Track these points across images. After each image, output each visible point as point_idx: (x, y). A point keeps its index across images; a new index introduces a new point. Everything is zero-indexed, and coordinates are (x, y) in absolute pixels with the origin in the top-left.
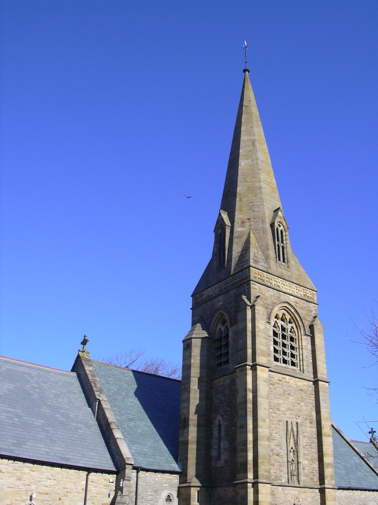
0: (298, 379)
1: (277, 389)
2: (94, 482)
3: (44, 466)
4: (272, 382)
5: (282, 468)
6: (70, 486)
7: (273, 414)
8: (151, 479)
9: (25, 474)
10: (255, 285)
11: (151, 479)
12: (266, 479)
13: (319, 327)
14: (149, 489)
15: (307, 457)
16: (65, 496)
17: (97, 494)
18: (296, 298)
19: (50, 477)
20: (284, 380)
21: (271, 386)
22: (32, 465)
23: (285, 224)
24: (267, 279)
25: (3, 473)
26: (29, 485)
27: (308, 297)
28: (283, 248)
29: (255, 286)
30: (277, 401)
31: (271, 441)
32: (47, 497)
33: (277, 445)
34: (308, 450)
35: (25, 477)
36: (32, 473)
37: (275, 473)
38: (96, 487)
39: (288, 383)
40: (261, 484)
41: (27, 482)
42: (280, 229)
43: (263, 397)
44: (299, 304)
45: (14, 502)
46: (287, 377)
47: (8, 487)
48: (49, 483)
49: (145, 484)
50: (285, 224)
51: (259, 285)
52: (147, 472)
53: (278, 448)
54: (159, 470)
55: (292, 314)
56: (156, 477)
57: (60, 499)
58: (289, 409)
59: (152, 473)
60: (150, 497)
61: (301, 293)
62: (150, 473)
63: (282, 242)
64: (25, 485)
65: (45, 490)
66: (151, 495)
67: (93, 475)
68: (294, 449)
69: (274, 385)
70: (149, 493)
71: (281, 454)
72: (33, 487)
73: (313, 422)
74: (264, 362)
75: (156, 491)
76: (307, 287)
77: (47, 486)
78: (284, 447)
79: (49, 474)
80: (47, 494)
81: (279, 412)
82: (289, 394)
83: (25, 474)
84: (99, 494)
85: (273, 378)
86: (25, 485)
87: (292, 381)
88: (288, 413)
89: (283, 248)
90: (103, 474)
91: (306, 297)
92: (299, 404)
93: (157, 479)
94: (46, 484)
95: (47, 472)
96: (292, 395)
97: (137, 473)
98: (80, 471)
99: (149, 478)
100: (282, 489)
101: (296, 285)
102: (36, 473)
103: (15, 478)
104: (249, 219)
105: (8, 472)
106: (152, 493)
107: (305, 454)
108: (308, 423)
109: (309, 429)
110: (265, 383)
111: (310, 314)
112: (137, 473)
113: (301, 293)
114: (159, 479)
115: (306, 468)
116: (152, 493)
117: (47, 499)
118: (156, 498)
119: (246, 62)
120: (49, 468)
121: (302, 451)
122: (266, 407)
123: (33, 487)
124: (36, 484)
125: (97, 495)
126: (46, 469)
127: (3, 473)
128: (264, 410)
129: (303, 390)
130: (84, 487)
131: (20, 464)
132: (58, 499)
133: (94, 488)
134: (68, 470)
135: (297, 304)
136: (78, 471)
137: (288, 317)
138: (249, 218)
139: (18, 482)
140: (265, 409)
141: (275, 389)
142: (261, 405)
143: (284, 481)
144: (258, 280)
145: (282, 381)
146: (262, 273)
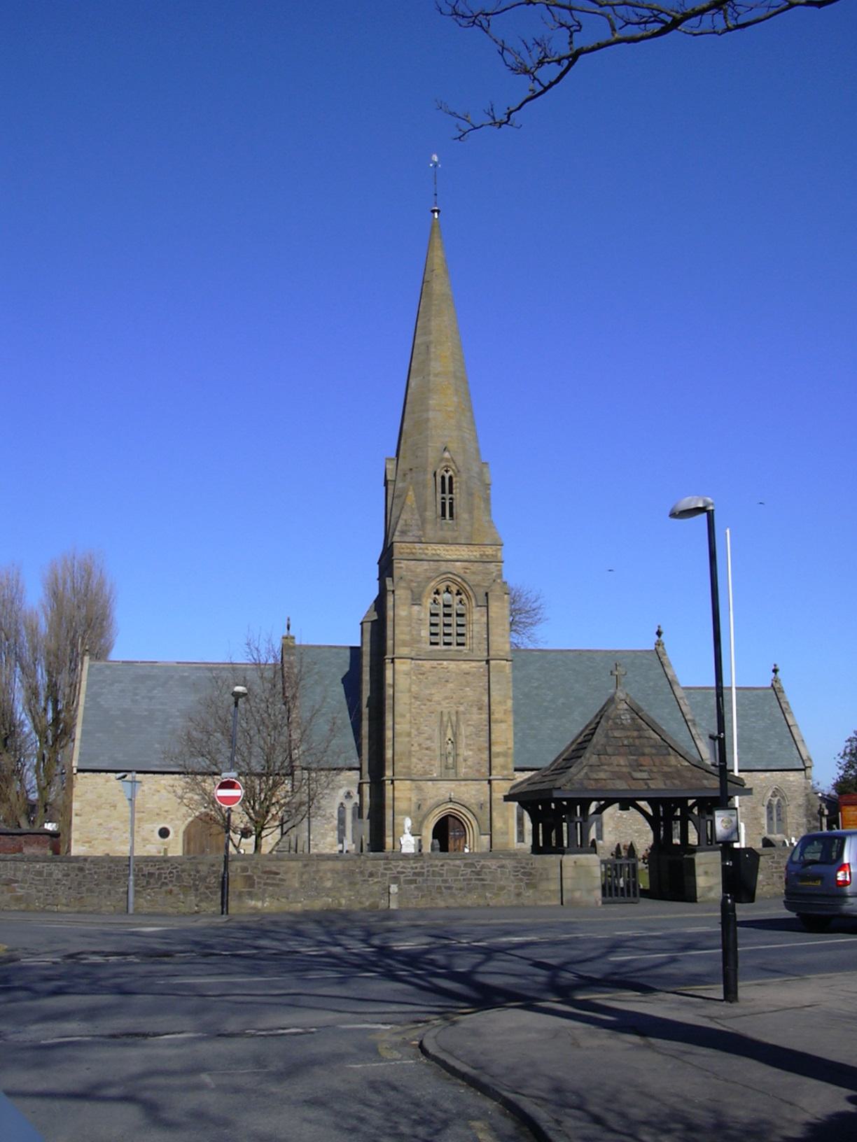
4: (421, 672)
5: (433, 762)
7: (423, 707)
10: (400, 563)
12: (404, 775)
13: (498, 593)
15: (471, 747)
20: (439, 667)
21: (421, 677)
23: (454, 468)
24: (421, 551)
27: (487, 556)
28: (451, 504)
29: (400, 565)
30: (428, 692)
33: (428, 739)
34: (473, 739)
37: (423, 767)
39: (447, 668)
40: (398, 782)
42: (447, 476)
43: (402, 692)
44: (470, 569)
46: (445, 663)
50: (454, 468)
53: (428, 742)
58: (446, 698)
61: (475, 553)
63: (451, 492)
68: (452, 739)
71: (432, 748)
73: (484, 708)
74: (406, 652)
78: (437, 740)
81: (431, 703)
87: (452, 665)
88: (444, 703)
89: (451, 504)
91: (484, 557)
92: (461, 690)
100: (433, 784)
104: (411, 469)
107: (468, 745)
108: (475, 710)
109: (475, 717)
113: (475, 553)
115: (470, 760)
119: (436, 195)
121: (463, 741)
137: (454, 589)
138: (411, 467)
140: (405, 704)
143: (435, 775)
144: (405, 556)
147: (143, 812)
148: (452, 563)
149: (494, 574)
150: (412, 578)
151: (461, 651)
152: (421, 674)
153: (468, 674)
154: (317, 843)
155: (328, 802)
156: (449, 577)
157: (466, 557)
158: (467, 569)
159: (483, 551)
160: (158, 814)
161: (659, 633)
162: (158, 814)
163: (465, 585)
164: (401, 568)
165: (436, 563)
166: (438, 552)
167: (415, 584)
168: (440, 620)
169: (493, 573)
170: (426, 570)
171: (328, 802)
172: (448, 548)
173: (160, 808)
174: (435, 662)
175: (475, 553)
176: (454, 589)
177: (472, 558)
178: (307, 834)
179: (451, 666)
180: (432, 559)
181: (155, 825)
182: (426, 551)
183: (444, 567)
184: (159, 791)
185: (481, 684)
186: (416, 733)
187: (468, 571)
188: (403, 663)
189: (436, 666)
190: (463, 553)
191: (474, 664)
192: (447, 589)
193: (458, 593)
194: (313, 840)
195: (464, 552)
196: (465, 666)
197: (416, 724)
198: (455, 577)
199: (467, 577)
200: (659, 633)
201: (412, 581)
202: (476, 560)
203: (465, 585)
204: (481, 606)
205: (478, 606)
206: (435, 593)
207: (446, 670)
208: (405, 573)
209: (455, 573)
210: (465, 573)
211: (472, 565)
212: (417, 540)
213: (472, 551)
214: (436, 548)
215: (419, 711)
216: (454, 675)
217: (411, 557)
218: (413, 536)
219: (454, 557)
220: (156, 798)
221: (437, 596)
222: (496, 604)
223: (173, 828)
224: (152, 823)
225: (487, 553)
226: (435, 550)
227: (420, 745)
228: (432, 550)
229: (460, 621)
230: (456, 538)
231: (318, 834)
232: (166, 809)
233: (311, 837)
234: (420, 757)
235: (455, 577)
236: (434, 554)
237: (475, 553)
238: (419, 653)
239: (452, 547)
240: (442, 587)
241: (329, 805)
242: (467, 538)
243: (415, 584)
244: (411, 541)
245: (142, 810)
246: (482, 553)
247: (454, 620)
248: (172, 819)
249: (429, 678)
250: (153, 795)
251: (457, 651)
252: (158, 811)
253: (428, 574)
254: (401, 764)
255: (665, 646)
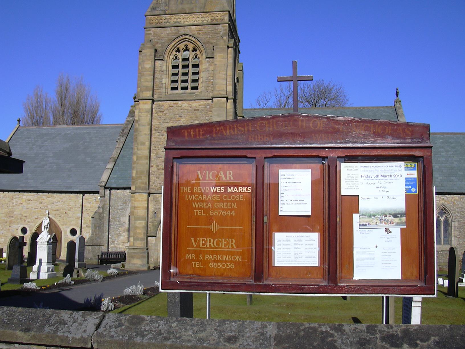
0: (194, 101)
1: (167, 114)
2: (88, 200)
3: (55, 194)
6: (72, 204)
7: (161, 137)
8: (121, 194)
9: (44, 200)
11: (121, 194)
14: (120, 201)
16: (69, 210)
17: (90, 207)
18: (198, 26)
19: (59, 200)
20: (175, 105)
21: (161, 114)
22: (48, 194)
25: (32, 200)
26: (47, 206)
31: (65, 172)
32: (58, 212)
35: (44, 201)
36: (48, 199)
38: (89, 203)
41: (45, 204)
43: (143, 125)
45: (39, 216)
46: (180, 102)
47: (35, 208)
48: (58, 203)
49: (116, 198)
51: (154, 29)
52: (118, 190)
54: (88, 194)
55: (194, 43)
56: (125, 192)
57: (66, 213)
59: (122, 190)
60: (120, 207)
61: (207, 19)
62: (120, 190)
64: (45, 206)
65: (57, 208)
66: (121, 206)
67: (87, 196)
69: (163, 112)
70: (120, 204)
72: (49, 207)
74: (148, 95)
75: (125, 203)
76: (214, 10)
77: (57, 206)
79: (58, 198)
80: (58, 210)
82: (181, 117)
83: (44, 200)
84: (92, 207)
85: (163, 106)
86: (45, 206)
87: (185, 104)
90: (94, 194)
93: (126, 194)
94: (57, 204)
95: (57, 197)
96: (185, 117)
97: (83, 195)
98: (78, 194)
99: (119, 194)
101: (200, 14)
102: (51, 198)
103: (38, 203)
105: (34, 200)
106: (122, 204)
110: (147, 113)
111: (217, 36)
112: (110, 191)
113: (207, 19)
114: (127, 194)
116: (122, 204)
117: (58, 213)
118: (125, 207)
120: (58, 194)
122: (146, 133)
123: (49, 207)
124: (51, 205)
125: (90, 208)
126: (56, 195)
127: (32, 200)
128: (144, 135)
129: (198, 109)
130: (81, 204)
131: (41, 194)
132: (65, 213)
133: (88, 204)
134: (70, 194)
135: (199, 32)
136: (76, 194)
137: (191, 47)
139: (40, 205)
140: (145, 134)
141: (164, 115)
142: (141, 132)
144: (154, 25)
145: (173, 106)
146: (160, 17)
147: (12, 217)
148: (189, 27)
149: (221, 33)
150: (158, 41)
151: (194, 93)
152: (160, 112)
153: (198, 110)
154: (114, 240)
155: (122, 212)
156: (184, 38)
157: (200, 22)
158: (200, 31)
159: (214, 17)
160: (21, 219)
161: (397, 95)
162: (21, 219)
163: (198, 43)
164: (150, 34)
165: (176, 28)
166: (179, 20)
167: (160, 45)
168: (181, 70)
169: (220, 32)
170: (168, 34)
171: (122, 212)
172: (187, 17)
173: (22, 215)
174: (172, 102)
175: (207, 18)
176: (191, 47)
177: (205, 22)
178: (107, 234)
179: (184, 105)
180: (174, 25)
181: (19, 226)
182: (170, 21)
183: (182, 30)
184: (22, 203)
185: (207, 118)
186: (155, 157)
187: (200, 32)
188: (146, 103)
189: (173, 105)
190: (198, 19)
191: (202, 102)
192: (186, 48)
193: (194, 50)
194: (111, 239)
195: (199, 19)
196: (195, 104)
197: (155, 150)
198: (190, 38)
199: (200, 36)
200: (397, 95)
201: (158, 43)
202: (208, 23)
203: (198, 43)
204: (209, 58)
205: (207, 58)
206: (176, 51)
207: (180, 108)
208: (152, 38)
209: (191, 34)
210: (198, 33)
211: (204, 28)
212: (162, 13)
213: (205, 18)
214: (177, 17)
215: (159, 140)
216: (186, 111)
217: (158, 25)
218: (160, 10)
219: (191, 23)
220: (20, 208)
221: (177, 53)
222: (220, 54)
223: (29, 228)
224: (18, 224)
225: (217, 18)
226: (177, 19)
227: (158, 166)
228: (174, 19)
229: (194, 70)
230: (193, 8)
231: (115, 234)
232: (25, 215)
233: (110, 236)
234: (158, 175)
235: (190, 38)
236: (175, 22)
237: (207, 18)
238: (160, 95)
239: (189, 15)
240: (182, 46)
241: (123, 213)
242: (201, 8)
243: (160, 45)
244: (158, 14)
245: (12, 216)
246: (213, 18)
247: (191, 70)
248: (29, 222)
249: (167, 114)
250: (19, 206)
251: (190, 93)
252: (20, 216)
253: (169, 37)
254: (140, 181)
255: (401, 103)
